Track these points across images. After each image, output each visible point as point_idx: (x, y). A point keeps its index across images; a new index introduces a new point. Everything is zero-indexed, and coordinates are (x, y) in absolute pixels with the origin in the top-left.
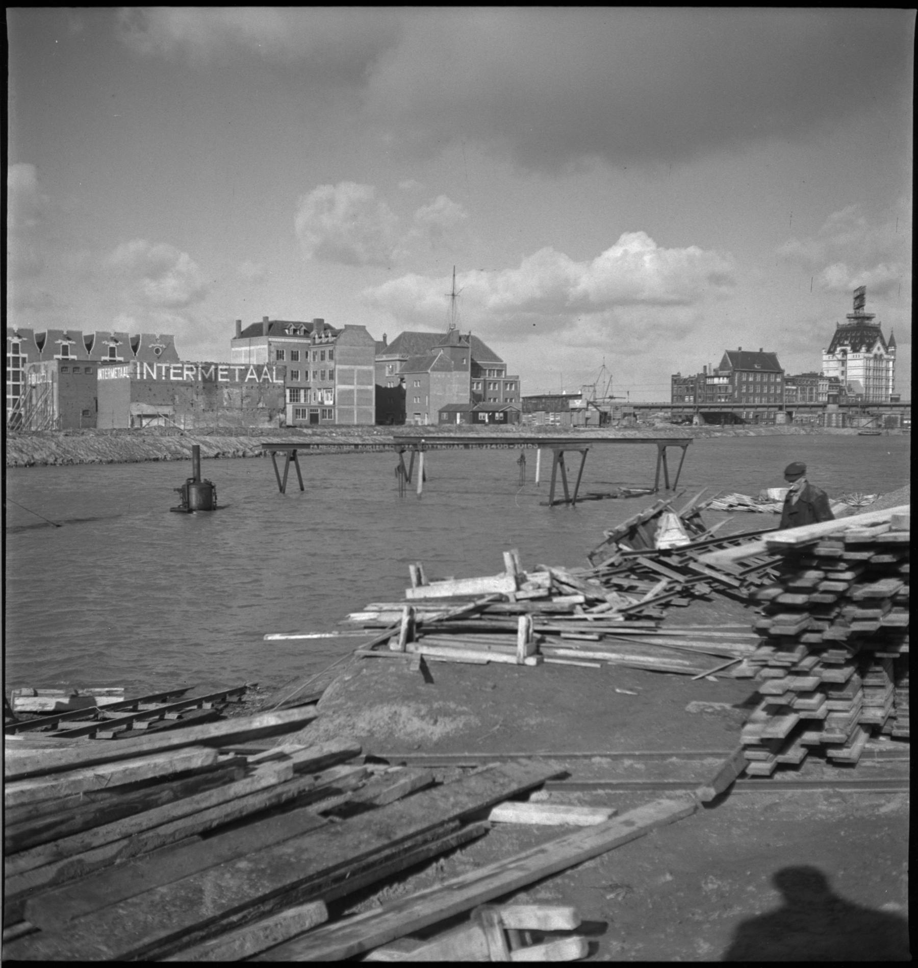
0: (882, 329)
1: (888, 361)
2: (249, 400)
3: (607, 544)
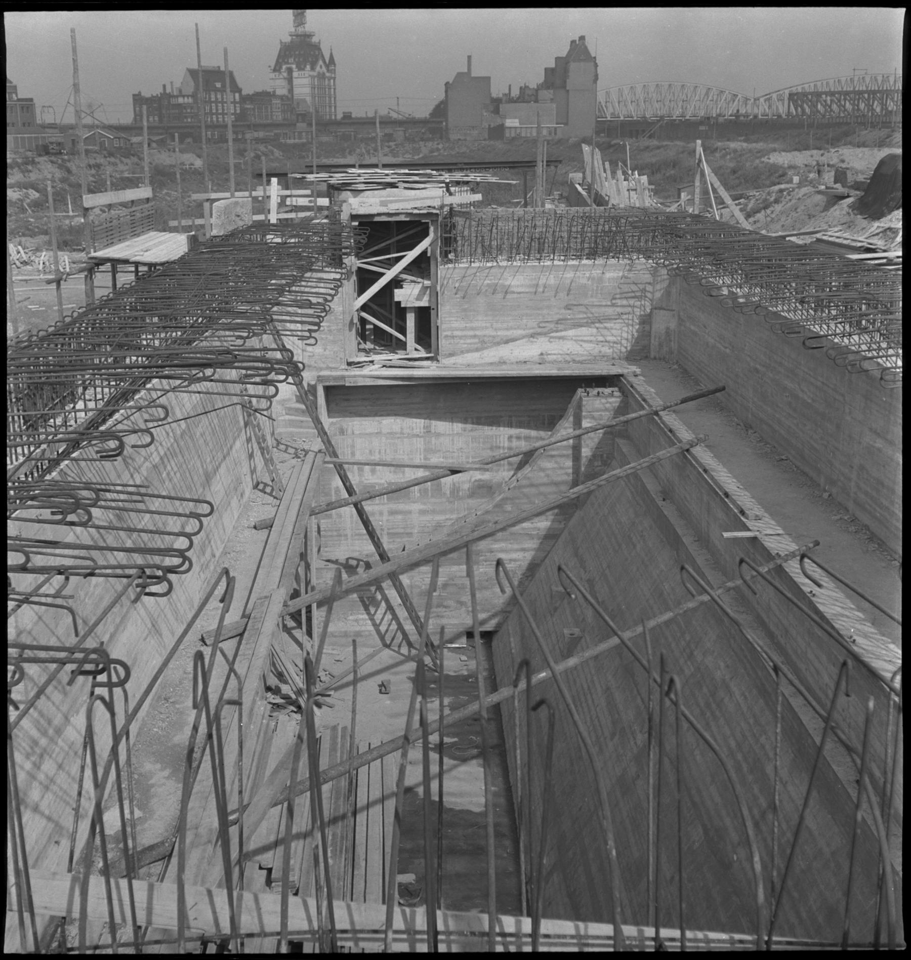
0: (322, 46)
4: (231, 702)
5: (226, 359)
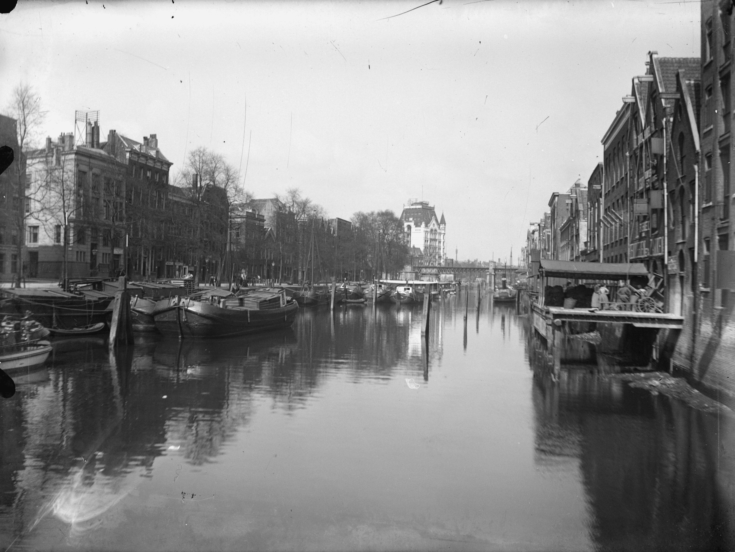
0: (436, 210)
1: (440, 234)
2: (62, 150)
3: (96, 121)
4: (631, 170)
5: (40, 345)
